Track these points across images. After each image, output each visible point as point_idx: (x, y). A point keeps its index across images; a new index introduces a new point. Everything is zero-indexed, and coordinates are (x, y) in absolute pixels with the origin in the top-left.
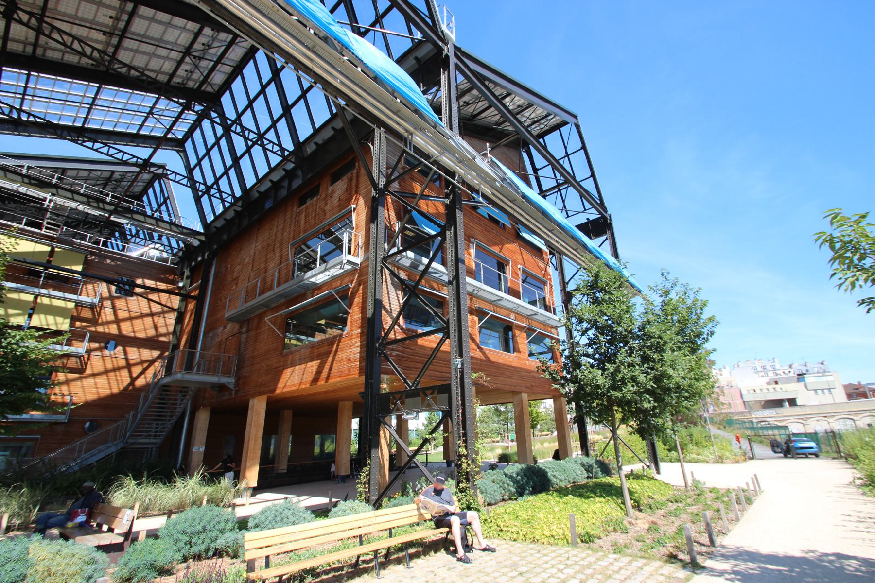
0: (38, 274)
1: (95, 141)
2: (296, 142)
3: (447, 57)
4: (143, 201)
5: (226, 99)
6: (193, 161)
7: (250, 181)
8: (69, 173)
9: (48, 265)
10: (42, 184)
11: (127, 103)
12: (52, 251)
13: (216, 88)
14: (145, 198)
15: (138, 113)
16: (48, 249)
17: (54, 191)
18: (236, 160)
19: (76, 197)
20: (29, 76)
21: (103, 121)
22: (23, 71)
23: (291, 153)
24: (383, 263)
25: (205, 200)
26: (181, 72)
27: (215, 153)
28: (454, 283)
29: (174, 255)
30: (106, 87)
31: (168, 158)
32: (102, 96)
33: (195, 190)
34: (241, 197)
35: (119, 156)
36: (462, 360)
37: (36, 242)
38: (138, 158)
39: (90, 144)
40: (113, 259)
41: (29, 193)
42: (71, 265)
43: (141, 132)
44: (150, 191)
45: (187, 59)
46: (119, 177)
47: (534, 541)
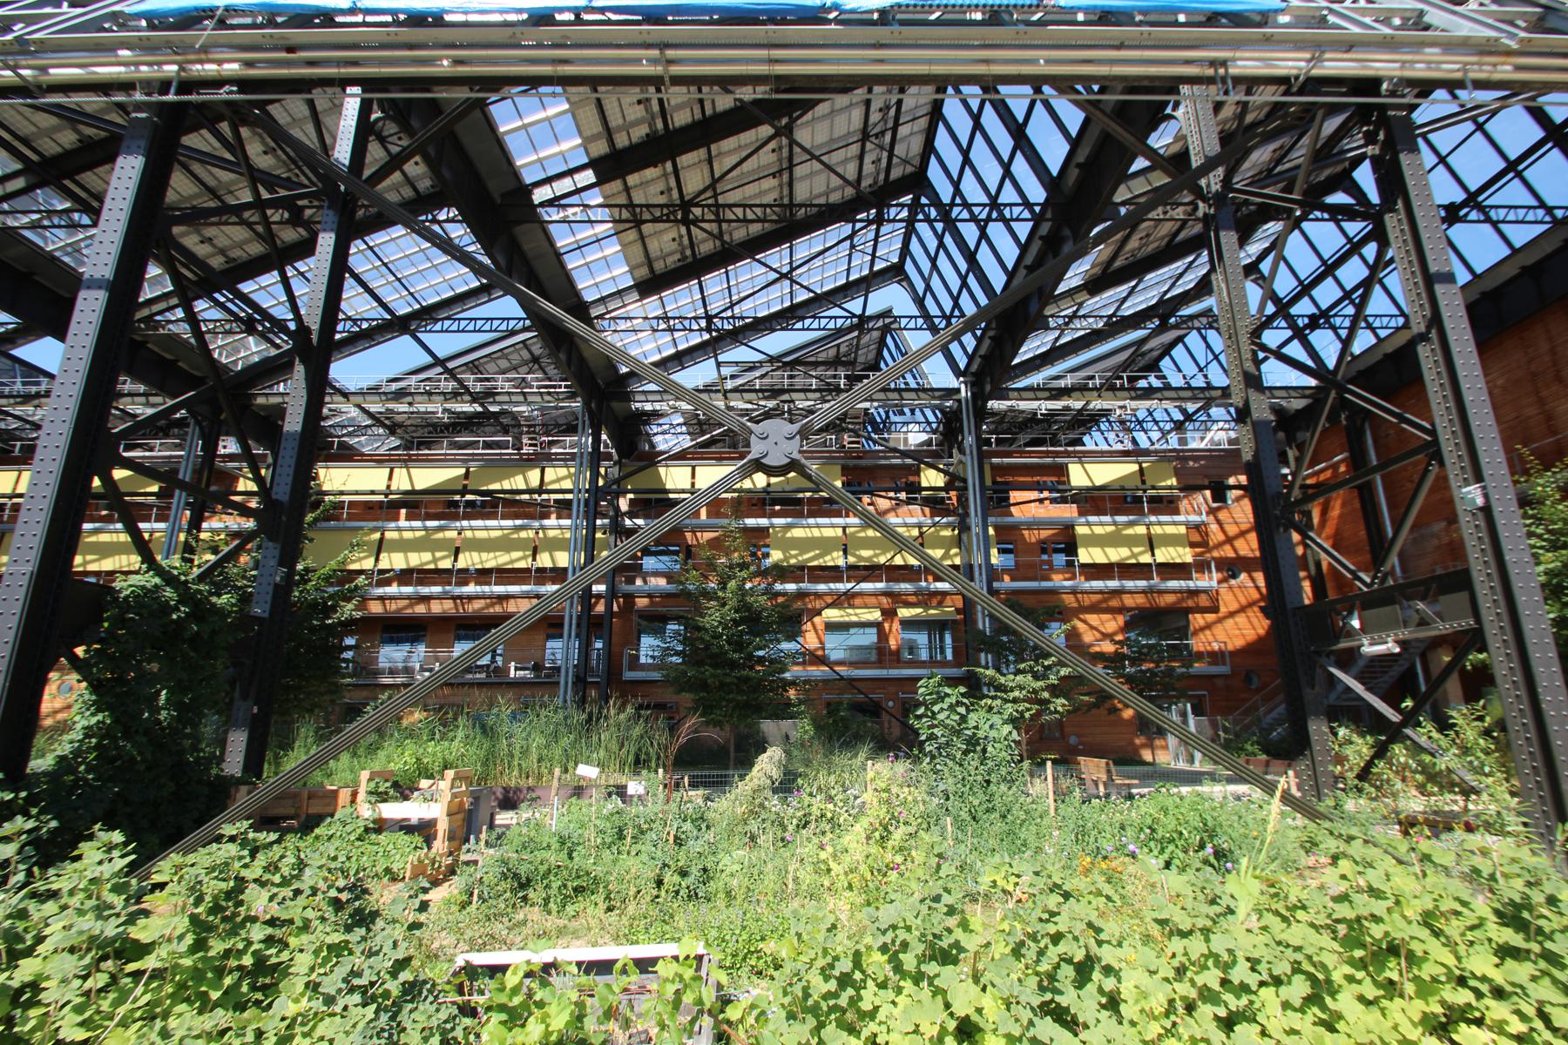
1: (803, 318)
2: (1047, 180)
5: (934, 173)
6: (920, 287)
7: (998, 280)
12: (1141, 469)
13: (917, 162)
16: (463, 471)
17: (409, 399)
18: (971, 257)
23: (1044, 206)
26: (868, 168)
27: (943, 261)
28: (1433, 334)
31: (891, 298)
35: (504, 327)
36: (1484, 488)
39: (799, 325)
40: (1196, 459)
42: (500, 480)
44: (885, 353)
45: (869, 146)
47: (1008, 1009)
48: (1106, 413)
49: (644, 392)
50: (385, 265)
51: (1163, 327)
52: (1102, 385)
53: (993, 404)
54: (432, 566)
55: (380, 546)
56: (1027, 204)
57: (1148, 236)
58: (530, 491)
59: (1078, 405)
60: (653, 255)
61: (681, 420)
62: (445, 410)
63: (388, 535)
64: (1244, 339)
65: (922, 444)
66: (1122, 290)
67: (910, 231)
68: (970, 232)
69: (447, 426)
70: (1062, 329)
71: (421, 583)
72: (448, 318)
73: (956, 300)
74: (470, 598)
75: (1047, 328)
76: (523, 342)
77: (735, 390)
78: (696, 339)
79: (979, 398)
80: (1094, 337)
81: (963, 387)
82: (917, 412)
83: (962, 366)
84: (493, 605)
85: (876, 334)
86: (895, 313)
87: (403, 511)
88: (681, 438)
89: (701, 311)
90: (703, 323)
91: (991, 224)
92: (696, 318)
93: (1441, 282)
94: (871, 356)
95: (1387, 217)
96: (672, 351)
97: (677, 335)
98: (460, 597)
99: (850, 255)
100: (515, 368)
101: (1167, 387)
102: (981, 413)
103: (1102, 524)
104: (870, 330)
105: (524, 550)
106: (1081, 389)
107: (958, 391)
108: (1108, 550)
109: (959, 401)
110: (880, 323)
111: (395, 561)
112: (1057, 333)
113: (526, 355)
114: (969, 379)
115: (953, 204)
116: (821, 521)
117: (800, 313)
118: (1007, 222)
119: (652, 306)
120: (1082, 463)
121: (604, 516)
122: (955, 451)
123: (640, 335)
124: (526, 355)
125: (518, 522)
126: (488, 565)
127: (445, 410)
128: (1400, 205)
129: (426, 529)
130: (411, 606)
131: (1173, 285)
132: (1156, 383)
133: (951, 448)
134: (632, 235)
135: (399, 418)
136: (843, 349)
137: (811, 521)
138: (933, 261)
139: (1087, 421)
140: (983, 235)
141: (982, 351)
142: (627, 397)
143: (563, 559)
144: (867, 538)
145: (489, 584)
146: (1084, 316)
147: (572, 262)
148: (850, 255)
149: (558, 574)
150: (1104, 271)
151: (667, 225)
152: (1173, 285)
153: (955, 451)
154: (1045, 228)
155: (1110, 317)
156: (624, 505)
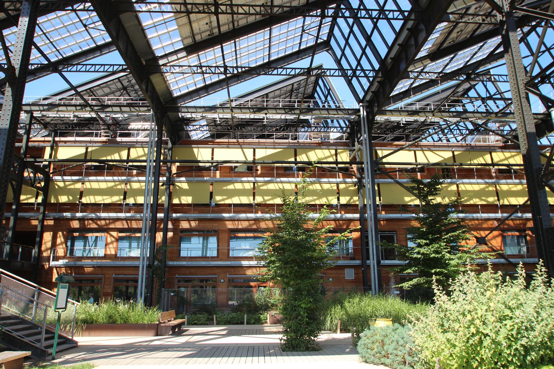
1: (276, 68)
6: (339, 53)
7: (383, 51)
8: (271, 95)
9: (212, 161)
10: (259, 110)
14: (316, 95)
17: (266, 111)
18: (368, 38)
20: (235, 42)
23: (410, 12)
25: (354, 81)
27: (352, 40)
30: (274, 27)
32: (273, 35)
34: (379, 68)
35: (111, 69)
37: (266, 148)
42: (110, 155)
44: (318, 89)
46: (297, 86)
48: (432, 124)
49: (187, 107)
50: (44, 34)
51: (468, 79)
52: (435, 109)
53: (379, 118)
56: (401, 12)
57: (461, 31)
58: (121, 161)
59: (422, 119)
60: (195, 32)
61: (205, 123)
62: (75, 116)
65: (337, 139)
66: (447, 59)
67: (334, 23)
68: (368, 25)
69: (76, 125)
70: (416, 78)
72: (77, 64)
75: (408, 77)
76: (118, 78)
78: (215, 79)
80: (432, 83)
81: (361, 108)
83: (361, 97)
86: (324, 67)
88: (205, 133)
89: (221, 63)
90: (222, 70)
91: (380, 21)
92: (218, 67)
96: (202, 85)
97: (206, 76)
99: (302, 35)
100: (113, 93)
101: (465, 111)
105: (119, 195)
107: (359, 110)
112: (413, 80)
113: (119, 85)
115: (359, 9)
116: (283, 179)
117: (274, 65)
118: (388, 20)
119: (193, 60)
121: (164, 175)
123: (186, 75)
124: (119, 85)
127: (75, 116)
131: (472, 57)
134: (185, 20)
135: (48, 120)
136: (295, 86)
137: (278, 180)
138: (347, 40)
139: (422, 128)
140: (375, 27)
141: (373, 89)
142: (177, 110)
143: (140, 200)
144: (489, 191)
146: (426, 72)
147: (150, 34)
148: (302, 35)
149: (138, 207)
150: (438, 49)
151: (204, 15)
152: (472, 57)
154: (410, 24)
155: (439, 73)
156: (174, 170)
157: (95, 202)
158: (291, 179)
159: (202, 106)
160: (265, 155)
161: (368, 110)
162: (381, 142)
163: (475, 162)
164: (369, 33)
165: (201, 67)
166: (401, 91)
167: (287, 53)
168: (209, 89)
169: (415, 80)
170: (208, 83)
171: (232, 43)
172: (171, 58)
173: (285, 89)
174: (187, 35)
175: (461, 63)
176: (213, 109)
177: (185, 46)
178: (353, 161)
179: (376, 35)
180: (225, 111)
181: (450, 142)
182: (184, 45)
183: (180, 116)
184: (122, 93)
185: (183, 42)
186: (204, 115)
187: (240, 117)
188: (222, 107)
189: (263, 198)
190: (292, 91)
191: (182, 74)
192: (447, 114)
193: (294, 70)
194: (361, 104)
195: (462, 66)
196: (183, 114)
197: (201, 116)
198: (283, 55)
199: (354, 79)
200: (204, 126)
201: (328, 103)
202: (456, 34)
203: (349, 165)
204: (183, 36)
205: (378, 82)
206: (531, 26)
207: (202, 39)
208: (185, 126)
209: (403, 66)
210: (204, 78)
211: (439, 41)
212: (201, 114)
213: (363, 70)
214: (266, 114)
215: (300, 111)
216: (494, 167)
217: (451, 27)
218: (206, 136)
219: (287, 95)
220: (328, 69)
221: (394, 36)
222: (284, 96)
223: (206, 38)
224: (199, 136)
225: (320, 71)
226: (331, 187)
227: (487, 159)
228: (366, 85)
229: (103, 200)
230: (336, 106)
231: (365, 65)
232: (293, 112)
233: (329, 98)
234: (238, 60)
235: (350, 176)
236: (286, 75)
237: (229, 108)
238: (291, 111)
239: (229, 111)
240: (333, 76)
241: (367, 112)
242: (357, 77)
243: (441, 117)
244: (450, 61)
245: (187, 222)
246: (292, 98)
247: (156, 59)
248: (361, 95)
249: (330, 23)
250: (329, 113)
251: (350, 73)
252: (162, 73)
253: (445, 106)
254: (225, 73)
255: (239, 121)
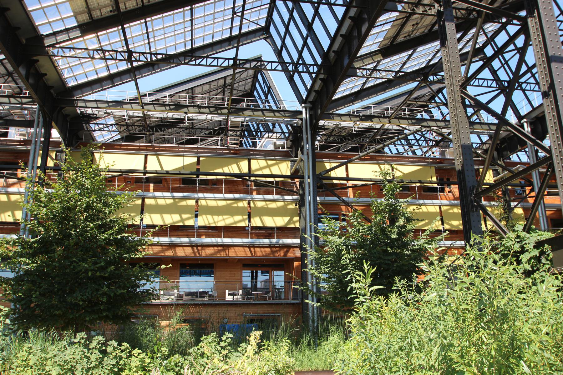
0: (193, 182)
3: (371, 277)
4: (255, 97)
6: (279, 43)
7: (325, 43)
8: (198, 90)
9: (198, 173)
10: (178, 107)
11: (215, 13)
12: (199, 161)
14: (255, 94)
15: (253, 10)
16: (195, 160)
17: (185, 110)
19: (202, 110)
20: (146, 22)
21: (204, 36)
22: (186, 8)
24: (462, 92)
25: (296, 77)
28: (551, 93)
29: (287, 139)
30: (196, 6)
32: (196, 16)
33: (285, 69)
34: (322, 63)
37: (184, 156)
38: (195, 65)
41: (175, 117)
42: (222, 167)
43: (233, 34)
44: (257, 85)
46: (231, 81)
49: (85, 101)
54: (181, 224)
55: (142, 210)
57: (417, 24)
61: (113, 122)
63: (148, 201)
64: (458, 89)
66: (404, 55)
71: (259, 236)
73: (300, 53)
74: (204, 246)
75: (355, 75)
77: (152, 103)
79: (314, 118)
81: (304, 110)
82: (277, 126)
84: (219, 251)
85: (251, 72)
87: (152, 185)
88: (114, 134)
90: (126, 55)
93: (555, 61)
94: (248, 87)
95: (529, 20)
97: (110, 62)
98: (197, 246)
99: (232, 19)
101: (432, 119)
102: (315, 129)
103: (164, 198)
104: (247, 69)
105: (242, 215)
106: (379, 116)
107: (301, 113)
108: (165, 216)
109: (301, 119)
110: (253, 64)
111: (156, 219)
114: (309, 105)
116: (427, 201)
117: (197, 54)
120: (157, 155)
122: (299, 152)
123: (83, 61)
125: (237, 196)
126: (219, 224)
128: (536, 14)
129: (173, 198)
130: (163, 251)
132: (426, 116)
133: (297, 151)
138: (287, 27)
140: (317, 13)
142: (73, 103)
144: (454, 213)
145: (220, 237)
148: (232, 19)
153: (299, 152)
157: (209, 224)
158: (435, 202)
159: (105, 100)
160: (182, 165)
161: (312, 112)
162: (335, 152)
163: (226, 170)
164: (310, 21)
165: (104, 51)
166: (352, 92)
167: (215, 39)
168: (115, 80)
169: (368, 78)
170: (113, 71)
171: (143, 23)
172: (60, 38)
173: (215, 83)
174: (81, 9)
175: (423, 62)
176: (119, 104)
177: (80, 23)
178: (295, 174)
179: (317, 23)
180: (135, 107)
181: (416, 155)
182: (78, 22)
183: (79, 111)
184: (6, 80)
185: (76, 18)
186: (109, 111)
187: (155, 116)
188: (132, 102)
189: (181, 217)
190: (225, 86)
191: (78, 59)
192: (406, 121)
193: (216, 60)
194: (303, 105)
195: (423, 66)
196: (82, 110)
197: (105, 113)
198: (210, 41)
199: (296, 74)
200: (112, 125)
201: (269, 103)
202: (412, 27)
203: (142, 174)
204: (75, 11)
205: (320, 79)
206: (501, 23)
207: (102, 15)
208: (84, 125)
209: (346, 61)
210: (108, 66)
211: (392, 34)
212: (104, 110)
213: (304, 64)
214: (186, 113)
215: (229, 111)
216: (198, 177)
217: (403, 18)
218: (115, 138)
219: (219, 91)
220: (269, 62)
221: (336, 25)
222: (215, 92)
223: (106, 15)
224: (107, 138)
225: (259, 64)
226: (267, 205)
227: (244, 166)
228: (309, 83)
229: (224, 219)
230: (277, 107)
231: (308, 60)
232: (219, 112)
233: (269, 97)
234: (152, 45)
235: (291, 192)
236: (217, 66)
237: (138, 103)
238: (217, 110)
239: (139, 107)
240: (275, 70)
241: (310, 115)
242: (299, 73)
243: (399, 124)
244: (408, 59)
245: (190, 248)
246: (226, 95)
247: (41, 38)
248: (304, 94)
249: (268, 6)
250: (264, 115)
251: (290, 68)
252: (50, 57)
253: (405, 110)
254: (130, 60)
255: (158, 121)
